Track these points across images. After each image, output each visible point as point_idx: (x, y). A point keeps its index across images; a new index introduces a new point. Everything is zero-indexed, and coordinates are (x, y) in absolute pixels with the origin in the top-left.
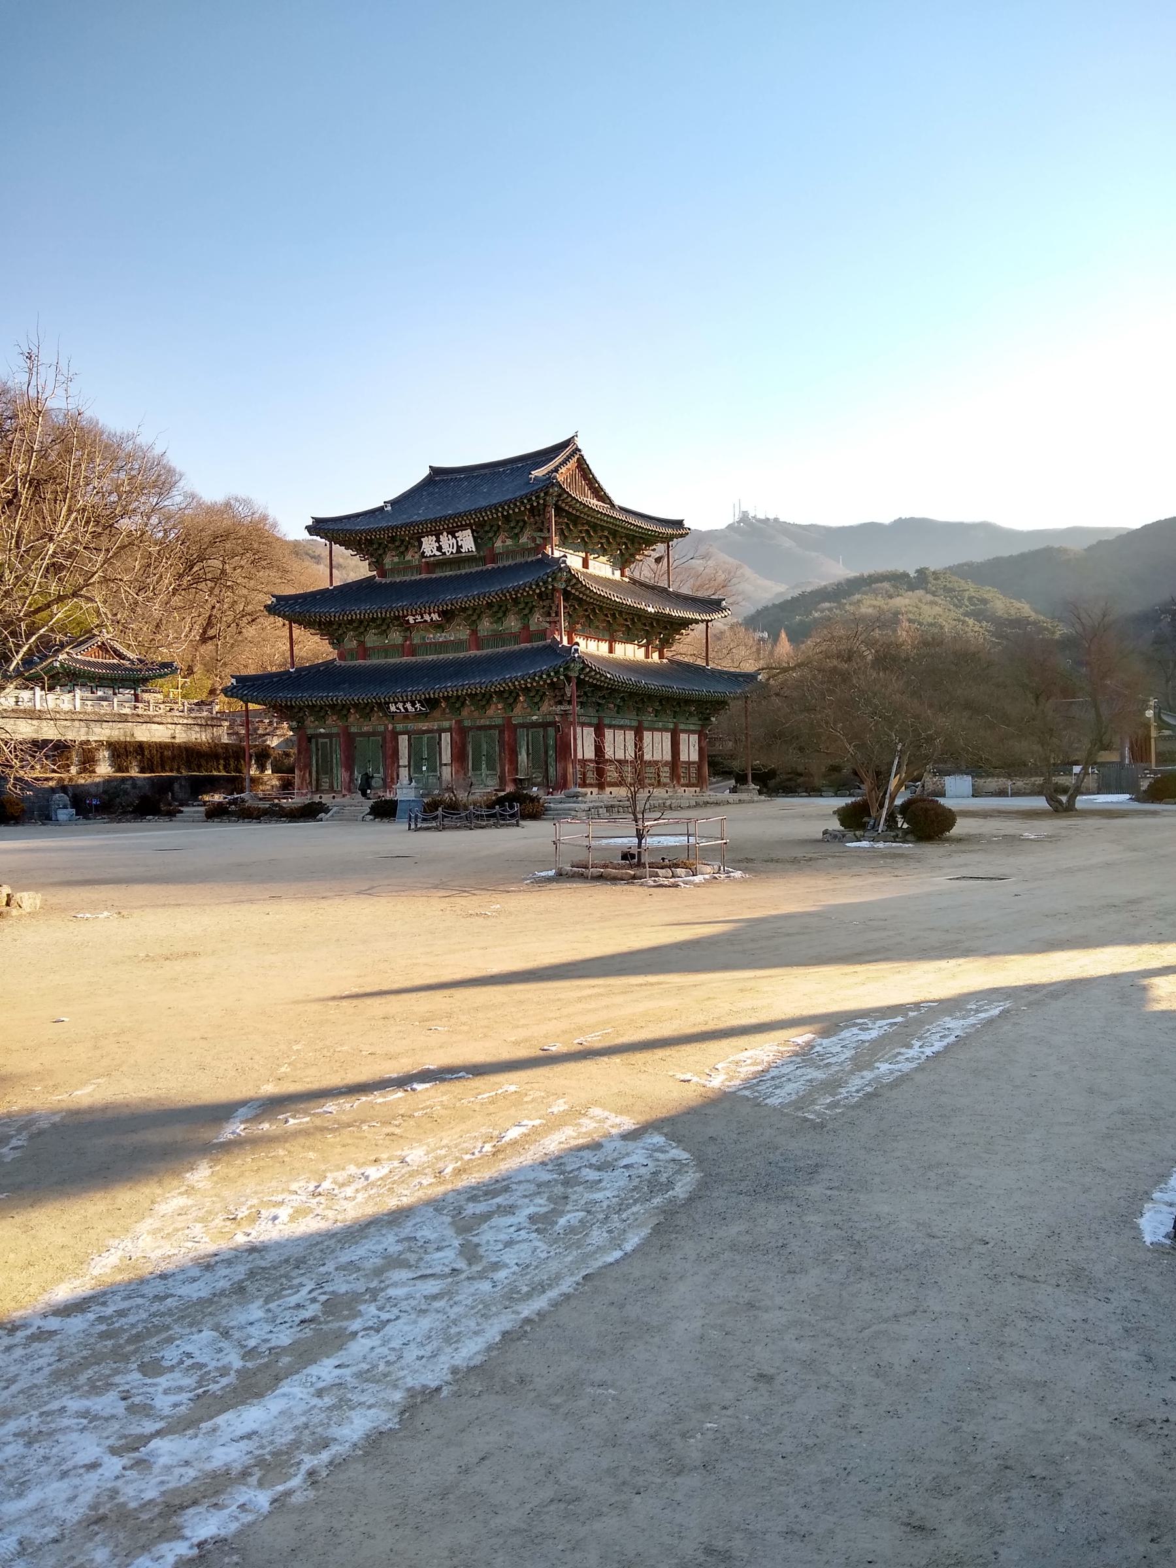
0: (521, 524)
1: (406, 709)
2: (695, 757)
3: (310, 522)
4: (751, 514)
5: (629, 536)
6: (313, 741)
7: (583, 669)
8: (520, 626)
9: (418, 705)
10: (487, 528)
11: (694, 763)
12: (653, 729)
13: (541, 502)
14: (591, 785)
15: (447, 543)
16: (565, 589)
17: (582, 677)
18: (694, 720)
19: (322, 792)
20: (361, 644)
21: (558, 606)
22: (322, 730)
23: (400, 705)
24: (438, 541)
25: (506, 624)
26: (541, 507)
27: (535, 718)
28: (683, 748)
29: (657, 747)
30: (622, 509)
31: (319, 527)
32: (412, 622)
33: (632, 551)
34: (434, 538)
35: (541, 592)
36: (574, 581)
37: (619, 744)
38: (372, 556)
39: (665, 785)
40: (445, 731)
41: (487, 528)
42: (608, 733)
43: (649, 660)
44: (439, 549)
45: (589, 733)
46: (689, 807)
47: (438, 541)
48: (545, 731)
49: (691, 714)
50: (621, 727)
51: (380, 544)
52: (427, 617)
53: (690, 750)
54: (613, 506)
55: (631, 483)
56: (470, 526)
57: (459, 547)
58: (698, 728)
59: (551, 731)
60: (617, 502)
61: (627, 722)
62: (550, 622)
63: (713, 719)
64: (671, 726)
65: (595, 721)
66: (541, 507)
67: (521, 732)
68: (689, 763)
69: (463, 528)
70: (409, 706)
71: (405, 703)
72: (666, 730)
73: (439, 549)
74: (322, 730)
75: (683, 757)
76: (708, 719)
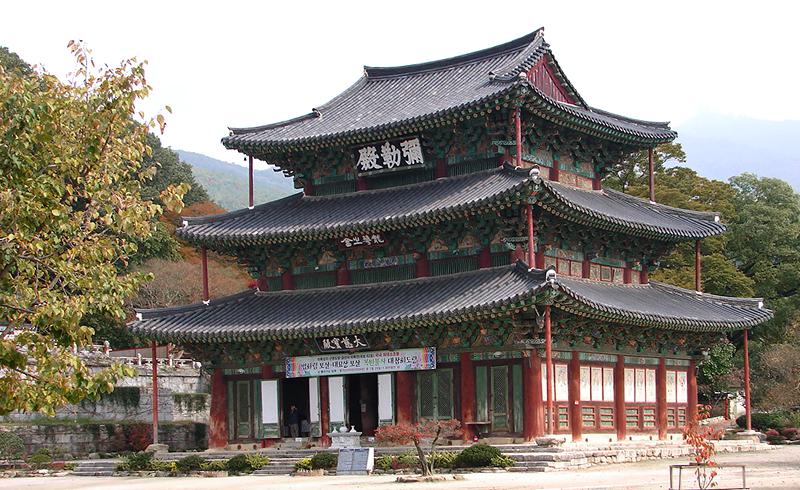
0: (479, 131)
1: (343, 345)
2: (683, 398)
3: (226, 134)
4: (144, 110)
5: (614, 147)
6: (231, 383)
7: (559, 297)
8: (479, 247)
9: (357, 341)
10: (438, 137)
11: (682, 405)
12: (634, 366)
13: (506, 105)
14: (564, 432)
15: (390, 156)
16: (535, 205)
17: (557, 306)
18: (684, 354)
19: (242, 441)
20: (288, 271)
21: (527, 224)
22: (241, 371)
23: (336, 341)
24: (379, 152)
25: (463, 246)
26: (504, 111)
27: (498, 354)
28: (670, 388)
29: (640, 388)
30: (595, 111)
31: (237, 141)
32: (348, 245)
33: (610, 158)
34: (374, 149)
35: (506, 208)
36: (547, 195)
37: (596, 387)
38: (299, 171)
39: (648, 431)
40: (562, 361)
41: (438, 137)
42: (584, 371)
43: (629, 285)
44: (380, 161)
45: (562, 371)
46: (578, 458)
47: (379, 152)
48: (511, 369)
49: (680, 348)
50: (601, 364)
51: (308, 157)
52: (367, 239)
53: (678, 391)
54: (586, 108)
55: (608, 87)
56: (418, 134)
57: (404, 159)
58: (687, 363)
59: (517, 369)
60: (590, 104)
61: (606, 358)
62: (515, 243)
63: (705, 353)
64: (656, 362)
65: (568, 356)
66: (504, 111)
67: (481, 372)
68: (676, 405)
69: (409, 137)
70: (346, 341)
71: (341, 338)
72: (651, 367)
73: (380, 161)
74: (241, 371)
75: (670, 398)
76: (699, 353)
